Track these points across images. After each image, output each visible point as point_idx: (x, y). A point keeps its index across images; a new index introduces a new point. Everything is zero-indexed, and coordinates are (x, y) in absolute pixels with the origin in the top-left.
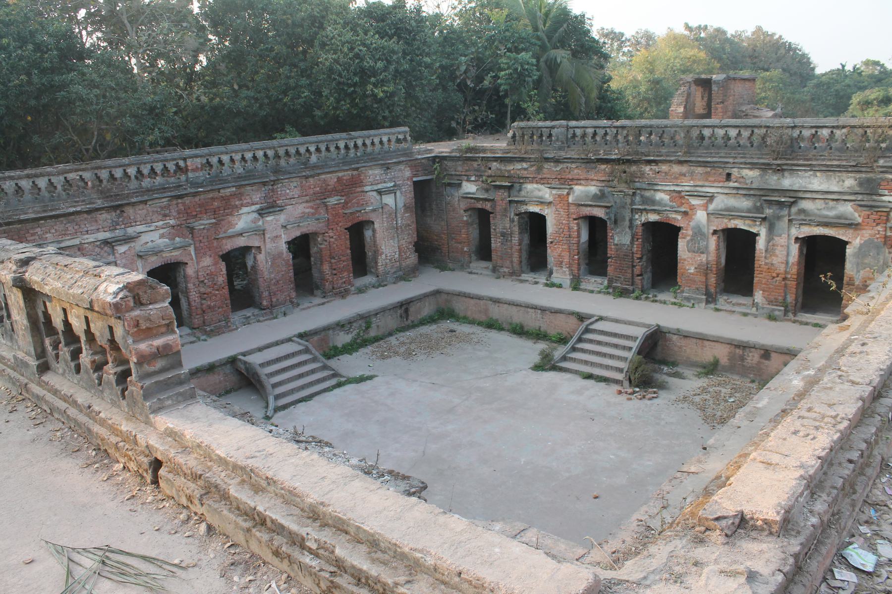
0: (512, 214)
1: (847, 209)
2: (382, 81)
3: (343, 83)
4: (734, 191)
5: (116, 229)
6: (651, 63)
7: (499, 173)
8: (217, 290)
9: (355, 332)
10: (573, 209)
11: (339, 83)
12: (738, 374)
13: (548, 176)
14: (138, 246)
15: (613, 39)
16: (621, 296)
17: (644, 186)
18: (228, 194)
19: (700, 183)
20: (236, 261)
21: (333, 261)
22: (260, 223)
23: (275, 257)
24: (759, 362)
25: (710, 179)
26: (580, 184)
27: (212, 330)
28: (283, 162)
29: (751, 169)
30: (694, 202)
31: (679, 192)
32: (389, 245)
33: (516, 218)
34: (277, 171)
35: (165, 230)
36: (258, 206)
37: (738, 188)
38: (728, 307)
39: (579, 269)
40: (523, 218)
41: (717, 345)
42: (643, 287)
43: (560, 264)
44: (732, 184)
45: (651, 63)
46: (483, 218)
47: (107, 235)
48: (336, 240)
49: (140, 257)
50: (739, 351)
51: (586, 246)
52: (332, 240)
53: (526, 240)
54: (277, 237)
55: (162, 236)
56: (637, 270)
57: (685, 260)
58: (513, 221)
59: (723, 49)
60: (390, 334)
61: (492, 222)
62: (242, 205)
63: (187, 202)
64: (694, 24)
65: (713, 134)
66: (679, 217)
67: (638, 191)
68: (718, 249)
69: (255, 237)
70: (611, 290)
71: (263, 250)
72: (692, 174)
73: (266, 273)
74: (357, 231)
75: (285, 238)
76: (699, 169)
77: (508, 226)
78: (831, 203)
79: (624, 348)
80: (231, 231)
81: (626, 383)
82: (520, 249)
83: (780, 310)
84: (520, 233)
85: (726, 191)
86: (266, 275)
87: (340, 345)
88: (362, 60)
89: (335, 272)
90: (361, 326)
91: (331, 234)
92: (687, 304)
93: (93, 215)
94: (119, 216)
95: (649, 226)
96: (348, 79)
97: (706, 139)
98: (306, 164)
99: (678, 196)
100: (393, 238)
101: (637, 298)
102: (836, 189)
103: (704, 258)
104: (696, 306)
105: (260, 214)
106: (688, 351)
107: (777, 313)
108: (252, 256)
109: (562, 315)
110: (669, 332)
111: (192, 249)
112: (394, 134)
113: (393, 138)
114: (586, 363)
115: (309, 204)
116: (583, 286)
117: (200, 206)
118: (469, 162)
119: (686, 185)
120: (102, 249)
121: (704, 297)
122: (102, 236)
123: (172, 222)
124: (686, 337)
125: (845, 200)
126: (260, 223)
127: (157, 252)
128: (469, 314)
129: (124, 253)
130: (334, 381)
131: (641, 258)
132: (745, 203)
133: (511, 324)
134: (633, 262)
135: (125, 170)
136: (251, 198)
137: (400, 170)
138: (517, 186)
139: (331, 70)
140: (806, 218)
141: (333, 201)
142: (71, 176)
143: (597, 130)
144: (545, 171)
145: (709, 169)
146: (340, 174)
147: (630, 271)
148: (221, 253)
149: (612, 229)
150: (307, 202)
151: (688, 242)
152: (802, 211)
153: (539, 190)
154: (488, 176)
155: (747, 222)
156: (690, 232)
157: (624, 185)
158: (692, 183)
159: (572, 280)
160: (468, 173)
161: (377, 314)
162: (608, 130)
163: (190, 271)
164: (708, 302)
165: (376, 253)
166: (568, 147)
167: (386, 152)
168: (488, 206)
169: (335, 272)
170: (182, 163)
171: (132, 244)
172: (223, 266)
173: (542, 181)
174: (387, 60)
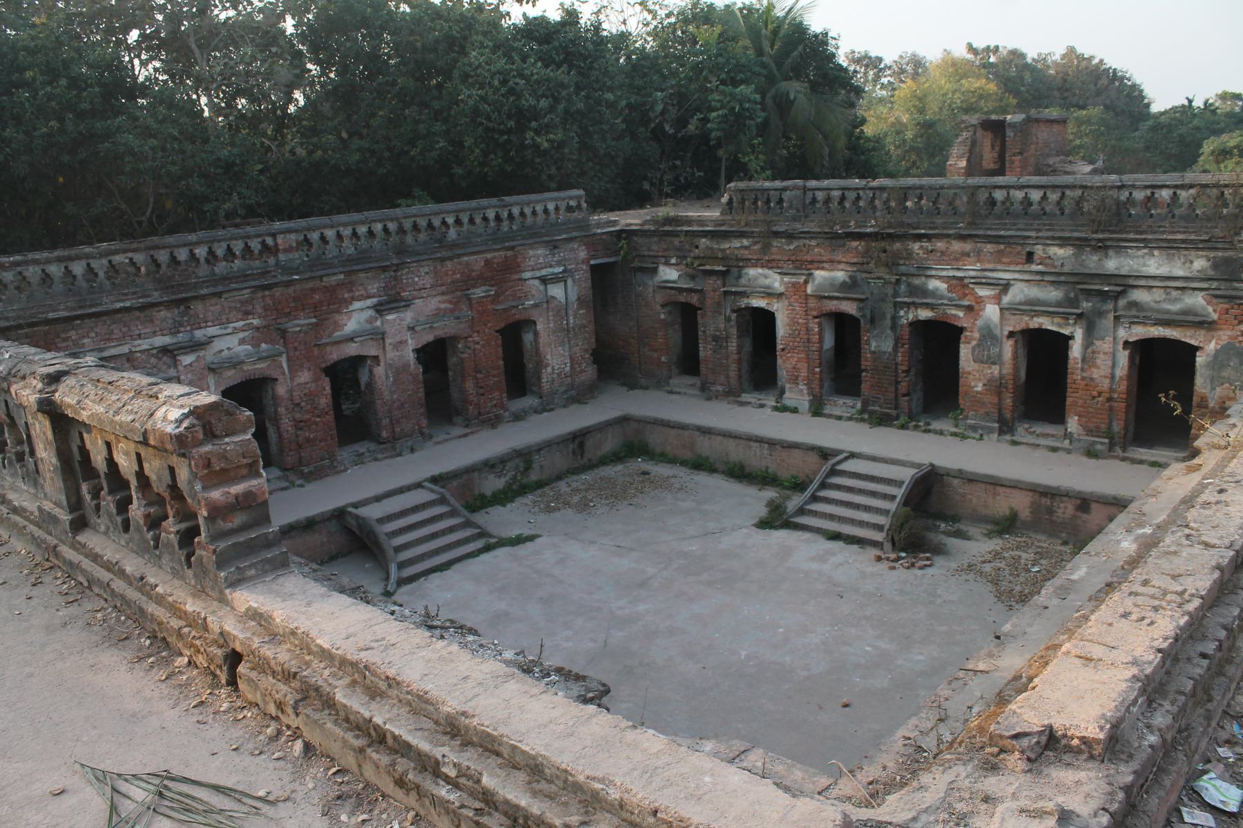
1: (1197, 301)
2: (547, 125)
3: (493, 130)
4: (1038, 278)
5: (179, 332)
6: (920, 99)
10: (812, 303)
11: (487, 129)
13: (778, 257)
14: (209, 355)
15: (867, 66)
17: (912, 271)
18: (334, 283)
19: (990, 266)
20: (346, 376)
21: (479, 376)
22: (378, 323)
23: (399, 371)
24: (1074, 517)
25: (1004, 260)
26: (823, 269)
27: (311, 472)
28: (409, 239)
29: (1061, 246)
30: (982, 292)
31: (961, 279)
32: (557, 355)
33: (734, 316)
34: (401, 251)
35: (246, 334)
36: (375, 300)
38: (1031, 439)
39: (821, 387)
41: (1016, 493)
42: (910, 410)
43: (795, 380)
44: (1034, 267)
45: (920, 99)
47: (165, 340)
49: (212, 370)
50: (1046, 501)
52: (478, 347)
54: (401, 342)
55: (242, 342)
56: (903, 387)
57: (969, 373)
59: (1022, 79)
60: (559, 478)
61: (700, 321)
62: (353, 299)
63: (277, 294)
64: (980, 44)
66: (961, 314)
68: (1015, 356)
69: (371, 343)
70: (866, 416)
72: (979, 253)
74: (513, 334)
75: (412, 344)
76: (989, 246)
77: (722, 326)
78: (1174, 293)
81: (888, 546)
83: (1102, 444)
84: (739, 337)
85: (1026, 277)
86: (387, 396)
87: (488, 493)
88: (519, 96)
89: (481, 391)
92: (973, 435)
93: (148, 312)
94: (183, 314)
95: (919, 326)
98: (441, 241)
99: (959, 284)
100: (562, 344)
102: (1180, 273)
103: (996, 370)
104: (985, 437)
106: (975, 500)
107: (1099, 447)
109: (797, 451)
110: (948, 475)
111: (283, 360)
112: (564, 199)
114: (832, 517)
115: (445, 298)
119: (971, 269)
120: (160, 359)
121: (996, 425)
122: (160, 341)
123: (256, 322)
124: (970, 481)
126: (378, 323)
127: (235, 363)
129: (191, 365)
130: (479, 544)
131: (907, 372)
132: (1054, 294)
133: (726, 463)
134: (896, 376)
135: (191, 251)
137: (572, 250)
138: (735, 270)
139: (476, 112)
140: (1140, 314)
141: (479, 292)
142: (118, 259)
143: (846, 193)
144: (774, 250)
145: (1002, 247)
146: (489, 256)
147: (892, 389)
148: (324, 365)
151: (973, 349)
152: (1134, 304)
153: (766, 277)
154: (695, 258)
155: (1056, 320)
156: (977, 335)
157: (883, 269)
158: (978, 266)
159: (812, 402)
160: (666, 254)
161: (540, 450)
162: (861, 192)
163: (281, 390)
164: (1001, 432)
165: (540, 364)
168: (694, 299)
169: (481, 391)
170: (269, 241)
171: (202, 353)
173: (770, 264)
174: (553, 96)
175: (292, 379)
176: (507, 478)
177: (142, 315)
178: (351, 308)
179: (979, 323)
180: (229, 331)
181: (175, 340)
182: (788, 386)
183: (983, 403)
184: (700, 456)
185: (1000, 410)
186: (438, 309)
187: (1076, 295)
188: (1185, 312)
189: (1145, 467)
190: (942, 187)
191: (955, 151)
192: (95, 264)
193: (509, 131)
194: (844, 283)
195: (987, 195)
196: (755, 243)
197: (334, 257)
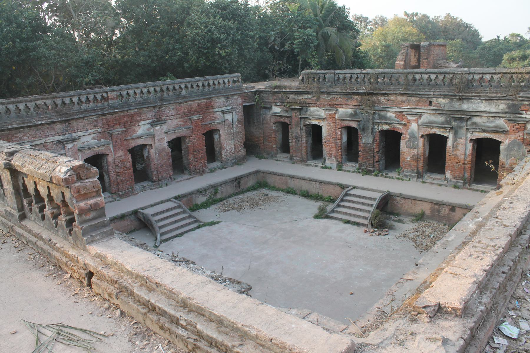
0: (302, 125)
1: (501, 122)
2: (225, 46)
3: (201, 47)
4: (434, 112)
5: (66, 134)
6: (384, 35)
7: (294, 101)
8: (126, 170)
9: (208, 196)
11: (199, 47)
12: (436, 220)
14: (79, 144)
15: (361, 21)
16: (366, 174)
17: (380, 109)
18: (133, 113)
20: (138, 153)
21: (195, 153)
22: (152, 130)
23: (161, 151)
24: (449, 214)
25: (419, 104)
26: (342, 108)
27: (123, 195)
29: (444, 98)
30: (410, 118)
31: (401, 112)
32: (229, 143)
33: (304, 128)
34: (162, 99)
35: (95, 135)
37: (434, 110)
39: (342, 158)
40: (308, 128)
43: (330, 155)
44: (432, 108)
45: (384, 35)
46: (285, 127)
48: (197, 140)
49: (80, 150)
50: (437, 207)
51: (346, 144)
52: (195, 141)
53: (310, 140)
54: (162, 139)
55: (93, 138)
58: (303, 130)
59: (427, 27)
61: (290, 130)
62: (141, 120)
63: (108, 118)
64: (410, 12)
65: (421, 78)
66: (401, 127)
67: (377, 112)
68: (424, 146)
69: (149, 139)
70: (360, 171)
71: (153, 146)
72: (409, 101)
73: (155, 160)
74: (210, 135)
75: (166, 139)
76: (413, 98)
77: (299, 132)
78: (491, 119)
79: (368, 205)
80: (134, 135)
81: (370, 226)
82: (307, 146)
83: (461, 183)
84: (306, 137)
85: (429, 112)
86: (155, 161)
87: (199, 203)
89: (196, 160)
90: (212, 192)
91: (194, 137)
93: (52, 125)
96: (204, 45)
97: (417, 80)
98: (179, 95)
99: (401, 114)
100: (231, 139)
101: (376, 175)
102: (494, 110)
103: (416, 151)
104: (411, 180)
105: (151, 125)
106: (406, 206)
107: (459, 184)
108: (147, 150)
110: (395, 196)
111: (111, 146)
112: (231, 78)
113: (231, 80)
114: (346, 214)
115: (180, 120)
116: (344, 168)
117: (116, 120)
118: (276, 95)
119: (405, 108)
120: (57, 146)
121: (416, 175)
123: (99, 130)
124: (405, 198)
125: (500, 117)
126: (152, 130)
127: (90, 148)
128: (276, 185)
129: (71, 148)
130: (195, 225)
131: (378, 152)
132: (440, 119)
133: (301, 191)
134: (373, 154)
135: (71, 99)
136: (146, 116)
137: (235, 99)
139: (194, 39)
140: (477, 128)
141: (195, 117)
142: (39, 102)
143: (352, 75)
144: (321, 99)
145: (419, 99)
146: (199, 102)
147: (372, 159)
148: (128, 149)
149: (361, 134)
150: (180, 118)
152: (474, 124)
153: (318, 111)
155: (442, 130)
156: (408, 136)
158: (409, 107)
160: (275, 101)
161: (221, 185)
162: (359, 75)
163: (110, 159)
165: (221, 148)
166: (335, 85)
167: (227, 88)
168: (287, 121)
169: (196, 160)
171: (76, 143)
172: (129, 156)
173: (320, 106)
174: (227, 33)
175: (115, 154)
176: (207, 197)
177: (50, 127)
178: (140, 124)
179: (409, 131)
180: (88, 134)
181: (64, 138)
182: (327, 158)
183: (410, 165)
184: (290, 188)
185: (417, 168)
186: (178, 124)
187: (450, 120)
188: (496, 127)
189: (478, 192)
190: (393, 73)
191: (399, 58)
192: (29, 104)
193: (208, 48)
194: (351, 114)
195: (412, 77)
196: (314, 97)
197: (133, 102)
